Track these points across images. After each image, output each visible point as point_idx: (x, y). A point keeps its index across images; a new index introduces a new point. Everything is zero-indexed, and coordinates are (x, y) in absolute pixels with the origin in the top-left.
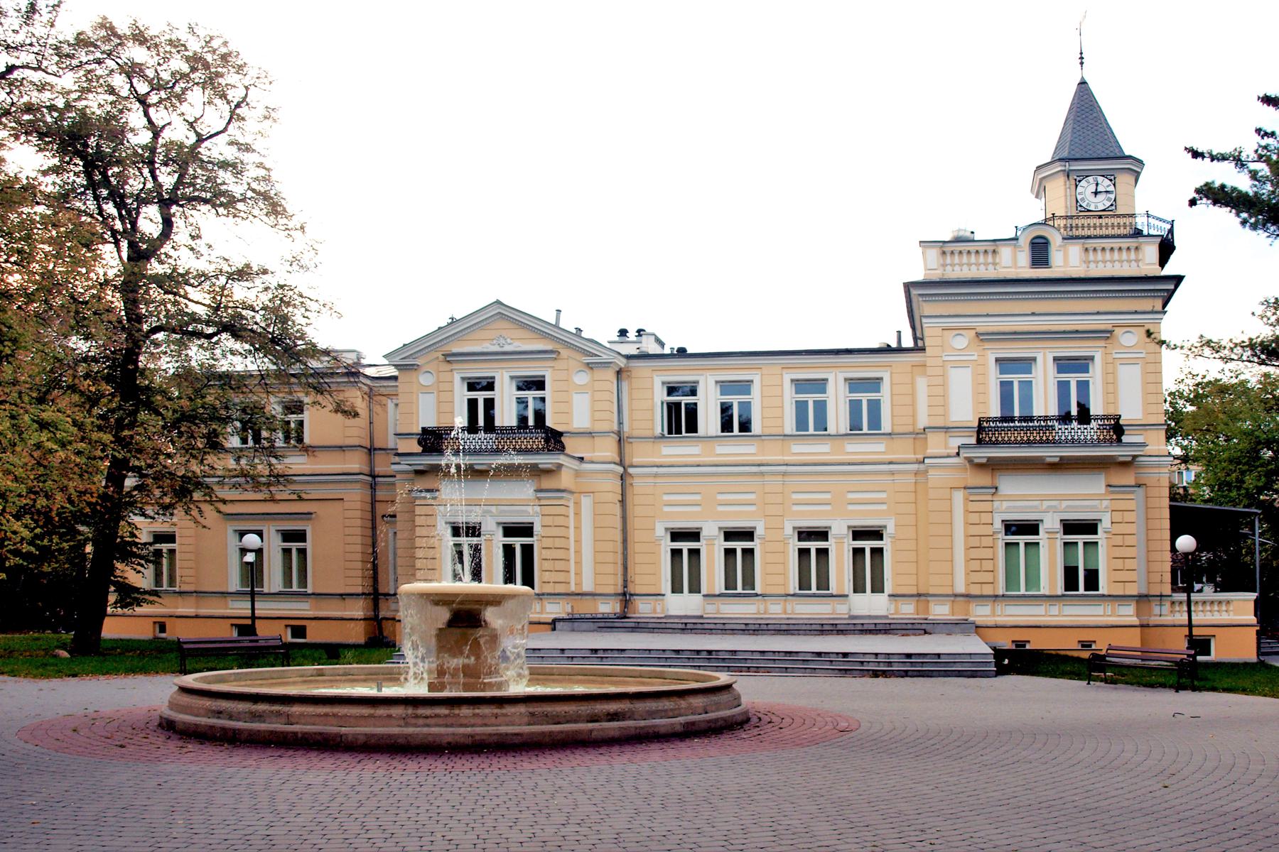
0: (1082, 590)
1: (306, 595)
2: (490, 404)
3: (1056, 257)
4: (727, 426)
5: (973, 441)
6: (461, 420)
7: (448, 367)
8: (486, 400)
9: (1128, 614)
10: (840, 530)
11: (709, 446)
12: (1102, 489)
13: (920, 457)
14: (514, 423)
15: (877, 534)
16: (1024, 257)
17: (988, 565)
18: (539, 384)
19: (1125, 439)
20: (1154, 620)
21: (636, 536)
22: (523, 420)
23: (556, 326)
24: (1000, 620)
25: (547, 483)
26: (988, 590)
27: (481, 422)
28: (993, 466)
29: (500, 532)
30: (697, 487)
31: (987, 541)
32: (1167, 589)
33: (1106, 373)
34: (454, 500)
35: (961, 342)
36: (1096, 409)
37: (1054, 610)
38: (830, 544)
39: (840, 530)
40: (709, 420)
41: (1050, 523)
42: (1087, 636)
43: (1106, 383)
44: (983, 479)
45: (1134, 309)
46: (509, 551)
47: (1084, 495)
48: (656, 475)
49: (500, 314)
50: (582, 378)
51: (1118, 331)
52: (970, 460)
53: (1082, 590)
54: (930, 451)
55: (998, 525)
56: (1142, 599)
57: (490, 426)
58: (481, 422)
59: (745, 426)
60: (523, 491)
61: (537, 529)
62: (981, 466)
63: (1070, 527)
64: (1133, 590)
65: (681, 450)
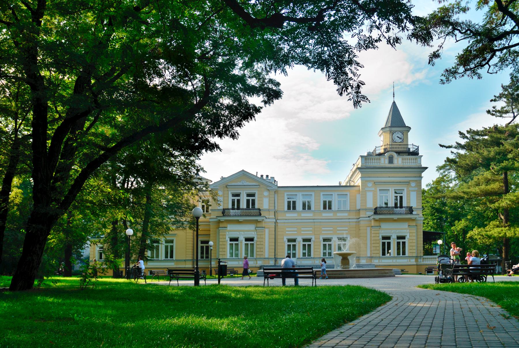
0: (169, 258)
1: (158, 260)
2: (238, 201)
3: (395, 161)
4: (304, 208)
5: (373, 213)
6: (230, 206)
7: (227, 189)
8: (237, 200)
9: (413, 261)
10: (299, 239)
11: (299, 213)
12: (407, 227)
13: (358, 217)
14: (394, 206)
15: (404, 238)
16: (387, 161)
17: (258, 250)
18: (253, 195)
19: (414, 213)
20: (419, 263)
21: (279, 241)
22: (396, 204)
23: (256, 176)
24: (381, 264)
25: (259, 225)
26: (378, 255)
27: (236, 207)
28: (380, 220)
29: (244, 240)
30: (296, 226)
31: (378, 242)
32: (422, 255)
33: (407, 194)
34: (233, 230)
35: (370, 185)
36: (405, 204)
37: (394, 261)
38: (391, 241)
39: (299, 239)
40: (299, 206)
41: (242, 239)
42: (403, 268)
43: (407, 197)
44: (377, 224)
45: (405, 176)
46: (398, 243)
47: (403, 229)
48: (320, 222)
49: (243, 174)
50: (266, 194)
51: (411, 182)
52: (374, 219)
53: (169, 258)
54: (361, 216)
55: (381, 237)
56: (417, 257)
57: (238, 208)
58: (399, 205)
59: (309, 208)
60: (252, 227)
61: (255, 239)
62: (376, 220)
63: (247, 240)
64: (415, 255)
65: (291, 215)
